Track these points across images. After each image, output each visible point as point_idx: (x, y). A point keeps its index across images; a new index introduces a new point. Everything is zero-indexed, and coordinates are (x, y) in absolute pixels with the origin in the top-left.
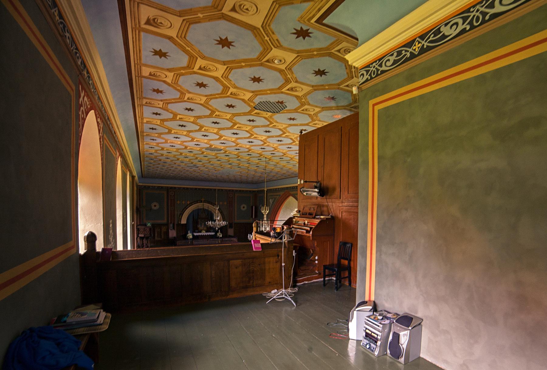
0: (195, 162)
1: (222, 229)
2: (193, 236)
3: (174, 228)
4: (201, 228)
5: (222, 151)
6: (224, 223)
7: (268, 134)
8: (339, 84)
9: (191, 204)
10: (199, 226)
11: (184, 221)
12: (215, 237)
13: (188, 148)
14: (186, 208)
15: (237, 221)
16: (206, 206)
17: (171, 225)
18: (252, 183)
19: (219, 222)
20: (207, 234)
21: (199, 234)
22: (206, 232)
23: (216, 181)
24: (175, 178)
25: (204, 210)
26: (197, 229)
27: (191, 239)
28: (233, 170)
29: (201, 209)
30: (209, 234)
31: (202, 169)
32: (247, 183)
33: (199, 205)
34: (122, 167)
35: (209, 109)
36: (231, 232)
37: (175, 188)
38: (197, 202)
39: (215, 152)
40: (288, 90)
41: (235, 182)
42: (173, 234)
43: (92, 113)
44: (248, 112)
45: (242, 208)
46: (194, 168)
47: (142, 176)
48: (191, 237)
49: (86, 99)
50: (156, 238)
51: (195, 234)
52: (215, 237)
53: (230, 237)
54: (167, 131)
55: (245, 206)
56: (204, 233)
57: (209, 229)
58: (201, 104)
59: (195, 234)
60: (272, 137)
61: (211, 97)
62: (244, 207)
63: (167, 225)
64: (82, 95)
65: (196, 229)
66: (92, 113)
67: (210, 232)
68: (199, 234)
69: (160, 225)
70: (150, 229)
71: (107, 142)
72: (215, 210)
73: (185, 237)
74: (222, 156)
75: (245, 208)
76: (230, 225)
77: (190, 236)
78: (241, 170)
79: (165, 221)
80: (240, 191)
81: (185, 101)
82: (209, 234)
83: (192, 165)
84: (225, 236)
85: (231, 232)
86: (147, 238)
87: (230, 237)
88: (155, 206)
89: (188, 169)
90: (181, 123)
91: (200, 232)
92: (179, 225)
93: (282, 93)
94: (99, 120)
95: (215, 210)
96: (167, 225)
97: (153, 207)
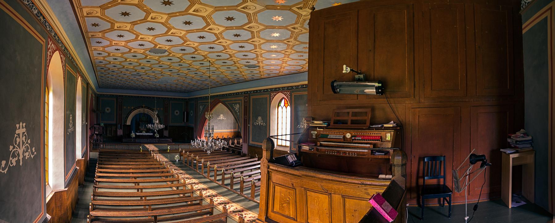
0: (139, 68)
1: (160, 131)
2: (136, 135)
3: (121, 128)
4: (141, 129)
5: (167, 53)
6: (162, 126)
7: (183, 52)
8: (237, 6)
9: (134, 109)
10: (140, 127)
11: (129, 123)
12: (153, 137)
13: (128, 60)
14: (130, 112)
15: (171, 124)
16: (147, 111)
17: (119, 126)
18: (185, 92)
19: (157, 125)
20: (146, 134)
21: (140, 134)
22: (146, 132)
23: (155, 90)
24: (122, 88)
25: (144, 114)
26: (139, 129)
27: (134, 138)
28: (170, 78)
29: (142, 113)
30: (148, 134)
31: (145, 77)
32: (181, 92)
33: (141, 110)
34: (82, 84)
35: (134, 34)
36: (166, 133)
37: (122, 96)
38: (139, 108)
39: (160, 55)
40: (194, 11)
41: (171, 91)
42: (120, 132)
43: (57, 54)
44: (165, 33)
45: (175, 113)
46: (138, 77)
47: (100, 86)
48: (134, 136)
49: (53, 45)
50: (108, 135)
51: (137, 134)
52: (153, 137)
53: (165, 137)
54: (107, 54)
55: (178, 112)
56: (144, 133)
57: (148, 130)
58: (127, 31)
59: (137, 134)
60: (187, 54)
61: (134, 23)
62: (177, 113)
63: (116, 125)
64: (50, 43)
65: (138, 130)
66: (57, 54)
67: (149, 132)
68: (140, 134)
69: (111, 125)
70: (103, 128)
71: (69, 68)
72: (154, 115)
73: (129, 136)
74: (164, 60)
75: (178, 113)
76: (166, 128)
77: (133, 135)
78: (179, 78)
79: (114, 122)
80: (174, 98)
81: (116, 30)
82: (148, 134)
83: (135, 73)
84: (162, 136)
85: (166, 133)
86: (101, 135)
87: (165, 137)
88: (108, 110)
89: (132, 77)
90: (117, 47)
91: (141, 132)
92: (125, 126)
93: (190, 14)
94: (62, 56)
95: (154, 115)
96: (116, 125)
97: (106, 111)
